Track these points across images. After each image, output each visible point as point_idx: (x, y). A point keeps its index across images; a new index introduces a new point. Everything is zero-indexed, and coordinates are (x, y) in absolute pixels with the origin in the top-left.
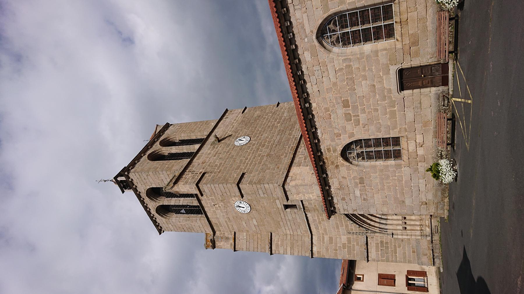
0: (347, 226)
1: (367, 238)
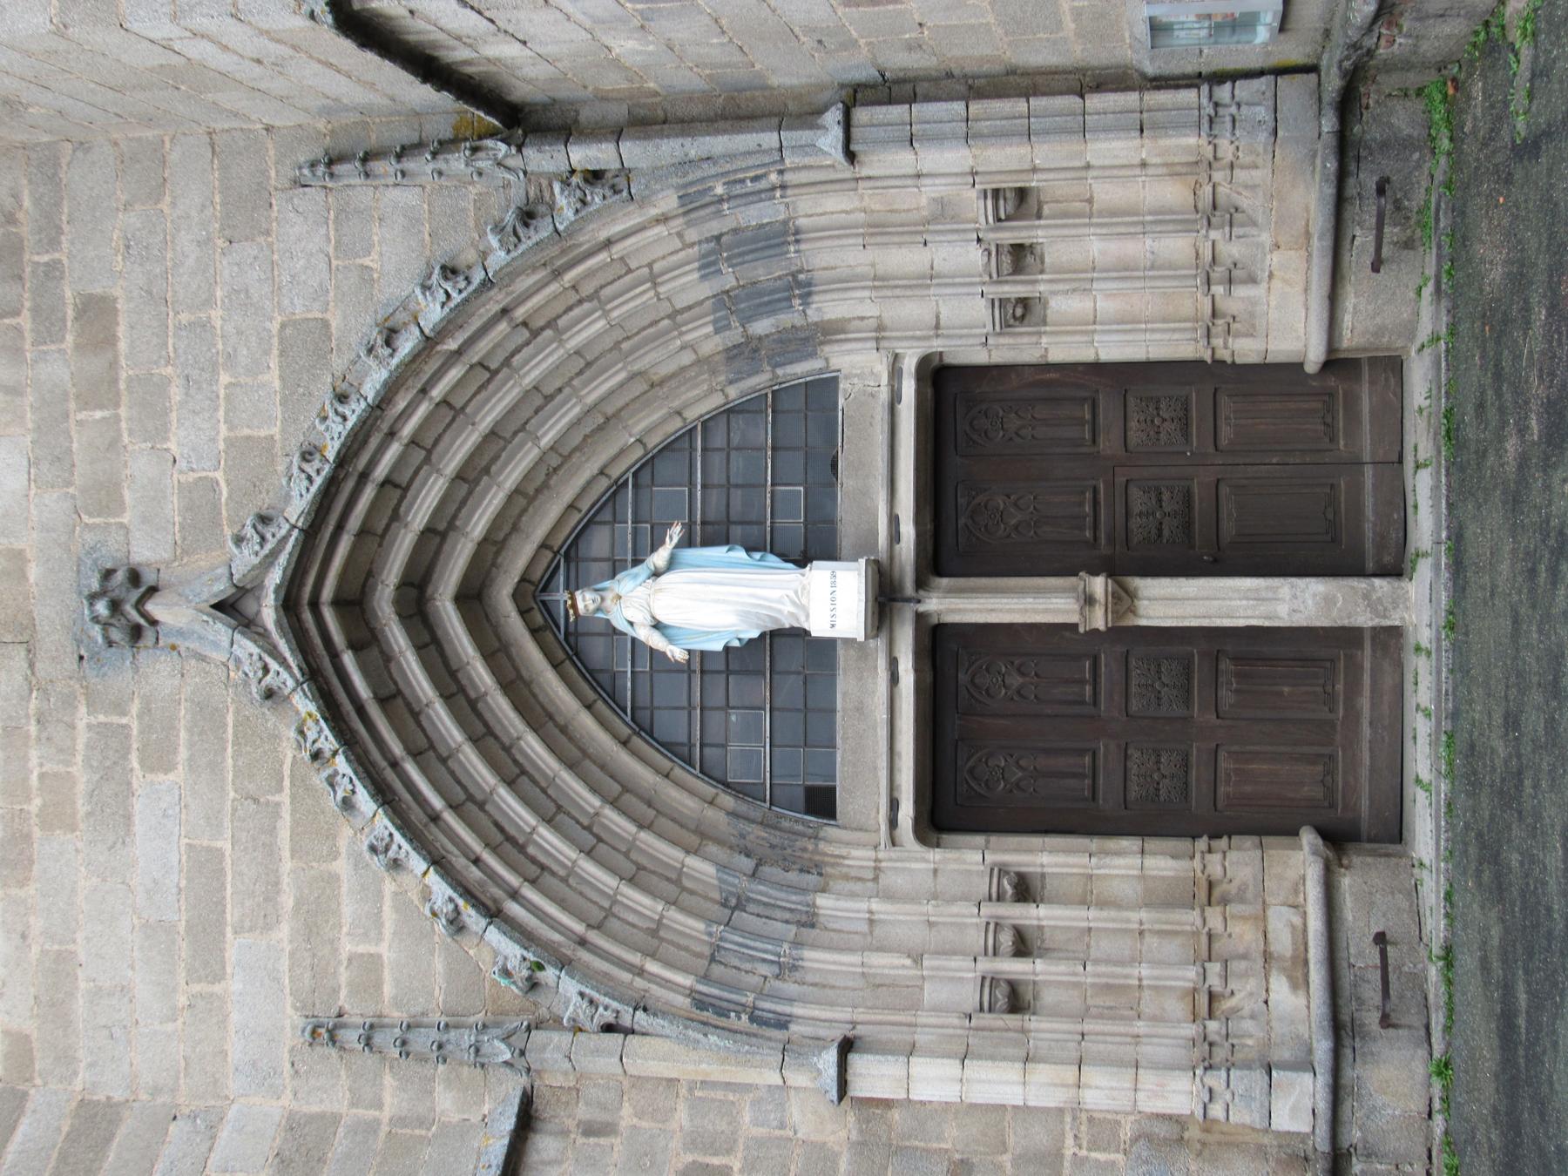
0: (315, 918)
1: (527, 1120)
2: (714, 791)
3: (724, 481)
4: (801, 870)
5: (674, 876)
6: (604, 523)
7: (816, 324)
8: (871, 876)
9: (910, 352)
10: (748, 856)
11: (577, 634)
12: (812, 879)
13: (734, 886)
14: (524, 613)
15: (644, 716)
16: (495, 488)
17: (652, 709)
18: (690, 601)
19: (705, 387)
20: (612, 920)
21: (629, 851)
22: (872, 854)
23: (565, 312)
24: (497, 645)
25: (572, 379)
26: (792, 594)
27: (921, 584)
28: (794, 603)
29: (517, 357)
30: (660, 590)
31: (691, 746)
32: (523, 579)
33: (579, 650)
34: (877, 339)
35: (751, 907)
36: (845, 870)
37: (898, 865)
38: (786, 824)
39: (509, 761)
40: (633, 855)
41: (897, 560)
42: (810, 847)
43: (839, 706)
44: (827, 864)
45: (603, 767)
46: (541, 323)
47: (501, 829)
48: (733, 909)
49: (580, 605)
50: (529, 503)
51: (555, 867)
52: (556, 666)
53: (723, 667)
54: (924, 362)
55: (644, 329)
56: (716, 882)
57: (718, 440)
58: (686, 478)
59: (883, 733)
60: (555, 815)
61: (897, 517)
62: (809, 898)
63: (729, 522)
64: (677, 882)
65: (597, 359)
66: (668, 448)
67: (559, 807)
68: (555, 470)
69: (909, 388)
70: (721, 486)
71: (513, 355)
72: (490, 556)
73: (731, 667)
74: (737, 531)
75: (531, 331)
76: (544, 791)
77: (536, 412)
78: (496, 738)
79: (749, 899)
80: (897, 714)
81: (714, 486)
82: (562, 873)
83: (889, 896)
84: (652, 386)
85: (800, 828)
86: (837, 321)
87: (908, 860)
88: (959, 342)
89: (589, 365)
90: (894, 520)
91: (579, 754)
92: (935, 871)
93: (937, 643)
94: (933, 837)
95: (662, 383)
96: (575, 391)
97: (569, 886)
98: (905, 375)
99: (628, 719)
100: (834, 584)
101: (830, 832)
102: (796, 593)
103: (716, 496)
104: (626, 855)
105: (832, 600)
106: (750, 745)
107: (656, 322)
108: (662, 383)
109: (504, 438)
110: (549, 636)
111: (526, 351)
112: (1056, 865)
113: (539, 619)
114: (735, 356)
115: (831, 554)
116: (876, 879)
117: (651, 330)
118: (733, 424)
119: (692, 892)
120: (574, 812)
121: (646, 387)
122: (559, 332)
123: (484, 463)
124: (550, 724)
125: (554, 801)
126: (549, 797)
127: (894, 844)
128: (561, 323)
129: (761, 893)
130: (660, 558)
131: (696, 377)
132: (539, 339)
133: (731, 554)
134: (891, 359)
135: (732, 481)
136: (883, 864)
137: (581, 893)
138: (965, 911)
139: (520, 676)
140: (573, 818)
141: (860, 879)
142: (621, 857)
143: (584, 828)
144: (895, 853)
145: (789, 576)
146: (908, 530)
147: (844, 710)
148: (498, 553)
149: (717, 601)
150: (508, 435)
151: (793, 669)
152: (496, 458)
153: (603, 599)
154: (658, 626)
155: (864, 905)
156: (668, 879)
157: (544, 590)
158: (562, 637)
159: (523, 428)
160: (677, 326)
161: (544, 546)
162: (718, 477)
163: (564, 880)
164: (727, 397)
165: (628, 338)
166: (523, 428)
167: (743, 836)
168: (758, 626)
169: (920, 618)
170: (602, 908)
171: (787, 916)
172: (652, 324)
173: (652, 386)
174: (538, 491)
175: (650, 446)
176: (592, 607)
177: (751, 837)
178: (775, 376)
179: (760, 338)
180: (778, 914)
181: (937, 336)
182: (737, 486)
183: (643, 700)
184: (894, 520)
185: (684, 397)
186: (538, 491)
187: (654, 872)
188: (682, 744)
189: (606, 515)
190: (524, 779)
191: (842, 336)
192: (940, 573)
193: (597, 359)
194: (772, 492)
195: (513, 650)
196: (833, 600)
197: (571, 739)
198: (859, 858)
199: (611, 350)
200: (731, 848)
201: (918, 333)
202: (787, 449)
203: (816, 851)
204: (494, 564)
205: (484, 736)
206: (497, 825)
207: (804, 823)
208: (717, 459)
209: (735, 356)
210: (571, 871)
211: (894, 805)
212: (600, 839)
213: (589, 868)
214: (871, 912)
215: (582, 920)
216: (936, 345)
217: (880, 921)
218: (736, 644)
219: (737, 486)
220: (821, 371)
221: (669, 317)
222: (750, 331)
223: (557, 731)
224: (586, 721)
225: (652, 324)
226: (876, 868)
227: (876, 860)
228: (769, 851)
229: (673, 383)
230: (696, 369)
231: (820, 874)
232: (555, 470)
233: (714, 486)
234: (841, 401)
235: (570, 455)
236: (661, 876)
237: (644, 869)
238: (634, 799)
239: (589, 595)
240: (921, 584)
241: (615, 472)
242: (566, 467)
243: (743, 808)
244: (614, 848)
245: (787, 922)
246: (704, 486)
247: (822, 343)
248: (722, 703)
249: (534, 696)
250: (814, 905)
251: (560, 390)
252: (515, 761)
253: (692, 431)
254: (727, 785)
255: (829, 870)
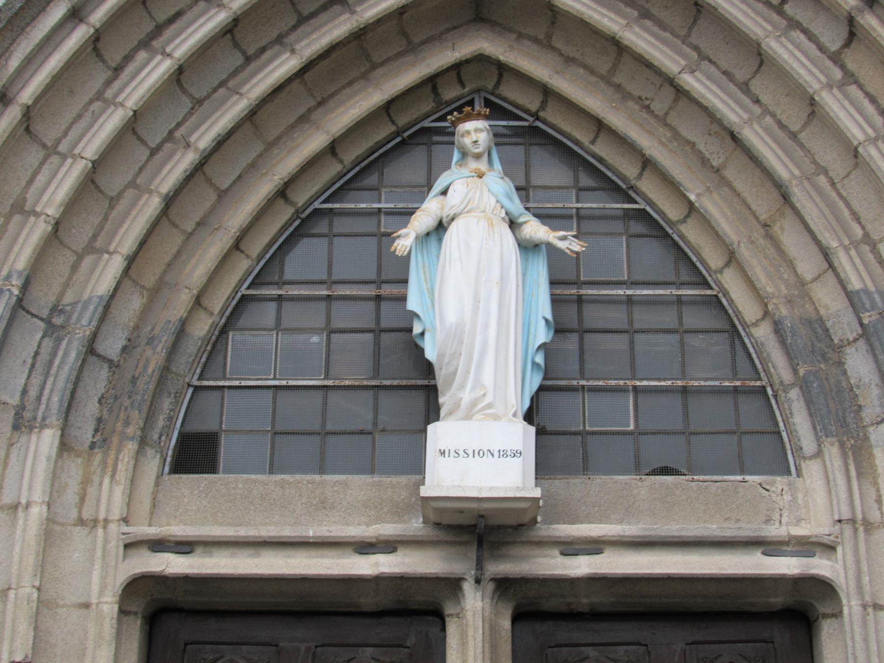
2: (217, 309)
3: (637, 326)
4: (99, 420)
5: (98, 244)
6: (576, 179)
7: (866, 438)
8: (86, 515)
9: (839, 566)
10: (124, 349)
11: (430, 144)
12: (85, 433)
13: (79, 319)
14: (457, 67)
15: (322, 227)
16: (624, 22)
17: (330, 236)
18: (475, 267)
19: (770, 290)
20: (41, 154)
21: (137, 187)
22: (116, 514)
23: (867, 94)
24: (416, 40)
25: (773, 115)
26: (488, 399)
27: (504, 586)
28: (474, 403)
29: (802, 37)
30: (492, 224)
31: (280, 284)
32: (503, 69)
33: (412, 138)
34: (853, 521)
35: (48, 344)
36: (96, 479)
37: (99, 552)
38: (166, 404)
39: (263, 43)
40: (130, 193)
41: (537, 551)
42: (130, 430)
43: (325, 477)
44: (106, 454)
45: (253, 165)
46: (851, 66)
47: (171, 20)
48: (48, 322)
49: (469, 126)
50: (602, 77)
51: (117, 84)
52: (388, 108)
53: (384, 324)
54: (823, 587)
55: (847, 204)
56: (86, 296)
57: (693, 319)
58: (637, 277)
59: (287, 532)
60: (190, 96)
61: (599, 552)
62: (55, 420)
63: (583, 332)
64: (91, 249)
65: (802, 146)
66: (680, 254)
67: (200, 102)
68: (647, 107)
69: (787, 566)
70: (631, 322)
71: (805, 31)
72: (530, 31)
73: (384, 336)
74: (572, 342)
75: (839, 52)
76: (222, 84)
77: (725, 73)
78: (295, 28)
79: (59, 340)
80: (314, 552)
81: (630, 314)
82: (109, 93)
83: (50, 535)
84: (765, 226)
85: (161, 423)
86: (873, 467)
87: (105, 567)
88: (858, 638)
89: (794, 136)
90: (594, 546)
91: (271, 138)
92: (87, 606)
93: (418, 609)
94: (138, 606)
95: (771, 237)
96: (759, 119)
97: (91, 102)
98: (805, 560)
99: (317, 205)
100: (503, 454)
101: (152, 464)
102: (489, 406)
103: (616, 317)
104: (132, 184)
105: (479, 451)
106: (275, 354)
107: (858, 219)
108: (771, 237)
109: (688, 35)
110: (427, 106)
111: (811, 47)
112: (25, 525)
113: (450, 92)
114: (814, 330)
115: (544, 467)
116: (81, 522)
117: (846, 212)
118: (716, 337)
119: (75, 268)
120: (193, 119)
121: (763, 217)
122: (841, 86)
123: (655, 11)
124: (313, 103)
125: (208, 96)
126: (215, 90)
127: (127, 546)
128: (853, 89)
129: (66, 354)
130: (535, 230)
131: (781, 278)
132: (828, 63)
133: (542, 323)
134: (826, 540)
135: (638, 337)
136: (100, 532)
137: (79, 116)
138: (18, 642)
139: (374, 67)
140: (185, 119)
141: (82, 499)
142: (129, 177)
143: (171, 133)
144: (116, 547)
145: (515, 396)
146: (581, 566)
147: (323, 483)
148: (535, 40)
149: (476, 299)
150: (693, 39)
151: (380, 417)
152: (663, 26)
153: (478, 157)
154: (441, 227)
155: (38, 495)
156: (95, 237)
157: (488, 103)
158: (426, 124)
159: (703, 57)
160: (856, 244)
161: (547, 92)
162: (643, 318)
163: (99, 96)
164: (755, 324)
165: (833, 184)
166: (703, 57)
167: (150, 341)
168: (441, 356)
169: (453, 585)
170: (58, 141)
171: (33, 393)
172: (853, 213)
173: (765, 226)
174: (618, 87)
175: (683, 228)
176: (467, 141)
177: (149, 353)
178: (786, 389)
179: (840, 364)
180: (36, 380)
181: (864, 607)
182: (632, 343)
183: (341, 225)
184: (594, 546)
185: (754, 262)
186: (618, 87)
187: (106, 218)
188: (282, 272)
189: (586, 180)
190: (241, 60)
191: (853, 473)
192: (517, 618)
193: (802, 146)
194: (622, 390)
195: (409, 58)
196: (480, 453)
197: (292, 127)
198: (111, 497)
199: (815, 162)
200: (137, 327)
201: (866, 579)
202: (685, 406)
203: (124, 437)
204: (521, 36)
205: (299, 13)
206: (178, 15)
207: (168, 428)
208: (668, 318)
209: (814, 330)
210: (112, 103)
211: (185, 547)
212: (154, 152)
213: (112, 122)
214: (28, 506)
215: (38, 99)
216: (851, 605)
217: (15, 520)
218: (417, 329)
219: (632, 343)
220: (798, 450)
221: (866, 235)
222: (849, 350)
223: (302, 110)
224: (314, 142)
225: (853, 213)
226: (95, 521)
227: (106, 521)
228: (128, 376)
229: (771, 251)
230: (793, 280)
231: (93, 446)
232: (647, 107)
233: (630, 314)
234: (754, 479)
235: (666, 125)
236: (101, 226)
237: (111, 207)
238: (208, 204)
239: (483, 138)
240: (504, 586)
241: (648, 186)
242: (652, 121)
243: (191, 347)
244: (141, 169)
245: (25, 392)
246: (630, 301)
247: (842, 445)
248: (336, 324)
249: (350, 84)
250: (43, 427)
251: (757, 101)
252: (263, 50)
253: (706, 284)
254: (224, 332)
255: (98, 457)
